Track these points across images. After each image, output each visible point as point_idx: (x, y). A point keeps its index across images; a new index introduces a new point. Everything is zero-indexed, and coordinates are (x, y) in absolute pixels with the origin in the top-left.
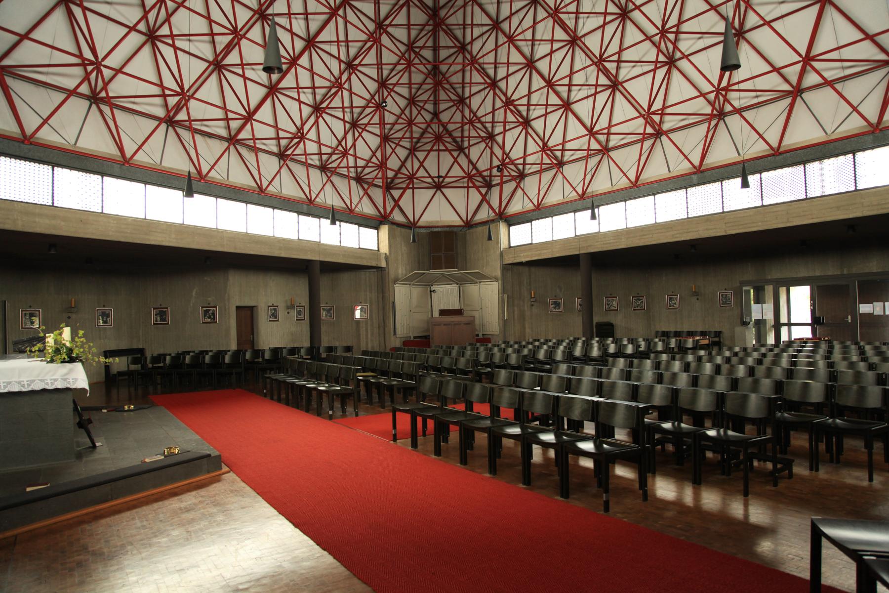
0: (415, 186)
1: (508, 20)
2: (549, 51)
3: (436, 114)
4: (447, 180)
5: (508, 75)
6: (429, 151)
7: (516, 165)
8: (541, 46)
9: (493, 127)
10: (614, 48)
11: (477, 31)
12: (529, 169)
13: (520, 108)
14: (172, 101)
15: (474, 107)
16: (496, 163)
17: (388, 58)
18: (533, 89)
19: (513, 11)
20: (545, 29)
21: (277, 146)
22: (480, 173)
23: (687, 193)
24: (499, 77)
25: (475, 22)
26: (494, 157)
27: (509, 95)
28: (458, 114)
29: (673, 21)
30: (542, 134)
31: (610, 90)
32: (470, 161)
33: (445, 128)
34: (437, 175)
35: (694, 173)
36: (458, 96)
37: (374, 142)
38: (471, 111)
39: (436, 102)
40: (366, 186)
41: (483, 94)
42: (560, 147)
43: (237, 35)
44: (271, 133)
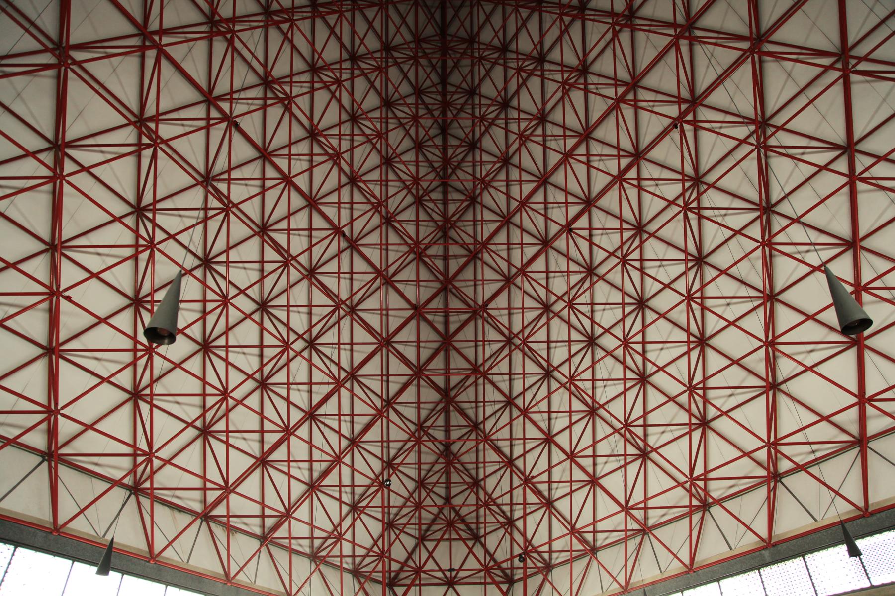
0: (422, 582)
1: (522, 396)
2: (568, 424)
3: (448, 499)
4: (462, 574)
5: (525, 453)
6: (439, 541)
7: (539, 553)
8: (558, 420)
9: (512, 510)
10: (638, 411)
11: (489, 410)
12: (557, 558)
13: (539, 486)
14: (212, 496)
15: (489, 488)
16: (517, 551)
17: (397, 434)
18: (553, 464)
19: (526, 387)
20: (560, 399)
21: (260, 527)
22: (498, 564)
23: (760, 575)
24: (515, 455)
25: (487, 399)
26: (515, 545)
27: (527, 473)
28: (473, 496)
29: (698, 378)
30: (568, 518)
31: (640, 461)
32: (487, 551)
33: (457, 513)
34: (449, 568)
35: (764, 548)
36: (471, 477)
37: (376, 528)
38: (486, 493)
39: (448, 486)
40: (363, 580)
41: (498, 475)
42: (590, 528)
43: (288, 432)
44: (256, 509)
